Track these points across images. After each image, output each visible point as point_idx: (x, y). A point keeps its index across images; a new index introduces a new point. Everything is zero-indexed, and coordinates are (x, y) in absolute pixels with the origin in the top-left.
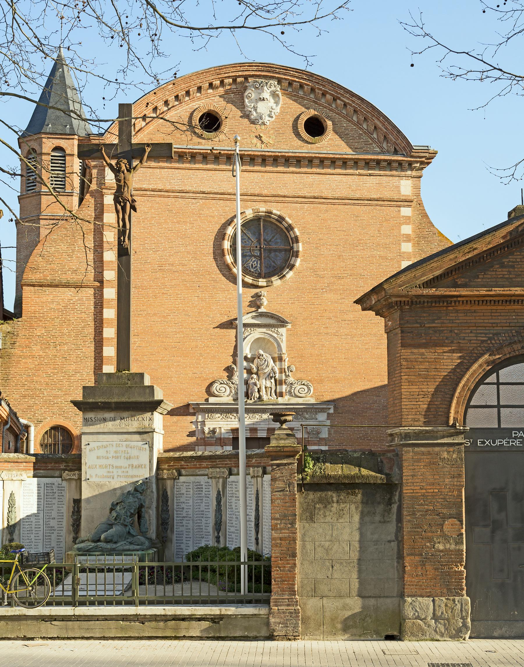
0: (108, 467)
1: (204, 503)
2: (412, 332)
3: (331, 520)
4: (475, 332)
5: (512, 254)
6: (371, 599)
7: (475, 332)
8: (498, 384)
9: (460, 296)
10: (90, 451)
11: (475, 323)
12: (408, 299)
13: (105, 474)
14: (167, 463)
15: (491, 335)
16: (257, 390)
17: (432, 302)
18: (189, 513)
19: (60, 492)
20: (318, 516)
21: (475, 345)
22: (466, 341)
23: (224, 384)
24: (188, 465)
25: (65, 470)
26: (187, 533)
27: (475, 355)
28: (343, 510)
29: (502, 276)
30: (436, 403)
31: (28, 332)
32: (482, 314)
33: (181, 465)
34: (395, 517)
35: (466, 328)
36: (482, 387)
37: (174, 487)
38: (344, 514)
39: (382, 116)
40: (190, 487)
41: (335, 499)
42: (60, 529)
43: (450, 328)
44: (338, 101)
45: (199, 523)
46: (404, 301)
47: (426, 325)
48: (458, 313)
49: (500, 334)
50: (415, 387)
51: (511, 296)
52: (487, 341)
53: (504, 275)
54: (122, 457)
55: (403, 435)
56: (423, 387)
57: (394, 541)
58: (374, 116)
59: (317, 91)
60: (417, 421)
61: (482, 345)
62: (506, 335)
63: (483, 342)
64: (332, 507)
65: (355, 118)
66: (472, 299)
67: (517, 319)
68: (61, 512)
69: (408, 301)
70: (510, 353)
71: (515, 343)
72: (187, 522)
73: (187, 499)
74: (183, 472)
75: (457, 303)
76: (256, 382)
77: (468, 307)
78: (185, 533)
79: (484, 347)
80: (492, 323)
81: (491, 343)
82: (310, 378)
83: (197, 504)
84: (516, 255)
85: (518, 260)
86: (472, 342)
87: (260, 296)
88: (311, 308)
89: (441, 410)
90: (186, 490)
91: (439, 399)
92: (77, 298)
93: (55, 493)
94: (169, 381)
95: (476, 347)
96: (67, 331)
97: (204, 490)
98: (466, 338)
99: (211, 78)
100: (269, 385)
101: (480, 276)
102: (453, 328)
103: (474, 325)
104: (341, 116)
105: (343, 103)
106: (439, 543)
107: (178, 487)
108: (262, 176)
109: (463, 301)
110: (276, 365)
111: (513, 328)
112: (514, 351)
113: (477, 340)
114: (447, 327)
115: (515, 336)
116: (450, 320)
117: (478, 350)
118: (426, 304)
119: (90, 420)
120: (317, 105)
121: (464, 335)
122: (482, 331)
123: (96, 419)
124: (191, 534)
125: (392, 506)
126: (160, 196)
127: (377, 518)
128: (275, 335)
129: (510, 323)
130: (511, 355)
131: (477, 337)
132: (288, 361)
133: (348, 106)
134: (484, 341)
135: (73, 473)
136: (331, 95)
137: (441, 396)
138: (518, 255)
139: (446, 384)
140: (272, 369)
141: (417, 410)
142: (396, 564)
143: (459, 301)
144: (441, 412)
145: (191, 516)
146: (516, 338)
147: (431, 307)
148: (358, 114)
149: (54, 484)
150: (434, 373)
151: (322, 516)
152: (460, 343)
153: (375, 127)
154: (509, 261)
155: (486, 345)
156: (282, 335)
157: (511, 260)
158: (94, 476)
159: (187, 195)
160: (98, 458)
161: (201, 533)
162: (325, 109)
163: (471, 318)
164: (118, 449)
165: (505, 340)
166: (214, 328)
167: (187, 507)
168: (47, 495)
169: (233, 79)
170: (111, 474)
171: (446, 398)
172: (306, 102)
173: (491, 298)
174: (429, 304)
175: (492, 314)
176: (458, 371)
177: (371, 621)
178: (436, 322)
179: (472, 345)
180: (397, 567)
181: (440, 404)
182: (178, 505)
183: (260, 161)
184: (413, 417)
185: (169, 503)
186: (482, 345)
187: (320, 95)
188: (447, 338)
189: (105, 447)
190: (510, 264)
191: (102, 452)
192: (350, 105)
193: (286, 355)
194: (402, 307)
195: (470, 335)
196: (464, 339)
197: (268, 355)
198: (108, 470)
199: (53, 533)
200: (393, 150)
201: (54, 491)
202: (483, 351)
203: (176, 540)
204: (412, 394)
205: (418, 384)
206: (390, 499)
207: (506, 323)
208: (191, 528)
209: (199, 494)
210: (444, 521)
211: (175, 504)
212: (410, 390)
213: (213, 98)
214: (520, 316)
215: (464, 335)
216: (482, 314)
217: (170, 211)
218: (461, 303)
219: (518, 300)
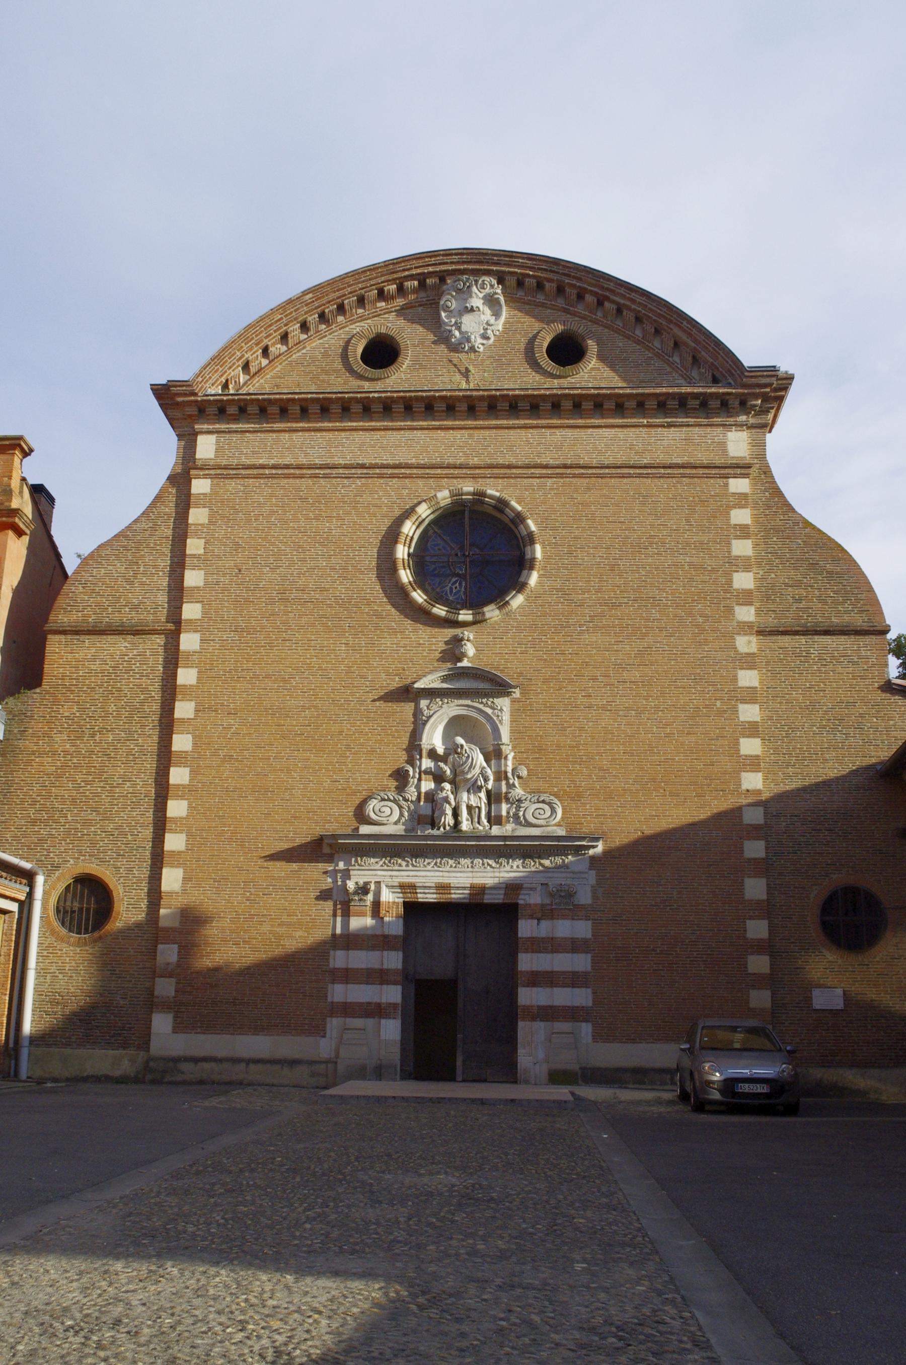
16: (449, 811)
23: (389, 800)
59: (568, 290)
65: (639, 332)
76: (447, 797)
82: (556, 790)
87: (462, 639)
88: (559, 661)
92: (135, 652)
100: (474, 802)
105: (615, 307)
108: (470, 436)
110: (489, 766)
128: (489, 711)
132: (514, 758)
140: (481, 773)
156: (501, 710)
166: (374, 701)
187: (574, 297)
192: (629, 309)
193: (510, 747)
197: (473, 746)
213: (386, 316)
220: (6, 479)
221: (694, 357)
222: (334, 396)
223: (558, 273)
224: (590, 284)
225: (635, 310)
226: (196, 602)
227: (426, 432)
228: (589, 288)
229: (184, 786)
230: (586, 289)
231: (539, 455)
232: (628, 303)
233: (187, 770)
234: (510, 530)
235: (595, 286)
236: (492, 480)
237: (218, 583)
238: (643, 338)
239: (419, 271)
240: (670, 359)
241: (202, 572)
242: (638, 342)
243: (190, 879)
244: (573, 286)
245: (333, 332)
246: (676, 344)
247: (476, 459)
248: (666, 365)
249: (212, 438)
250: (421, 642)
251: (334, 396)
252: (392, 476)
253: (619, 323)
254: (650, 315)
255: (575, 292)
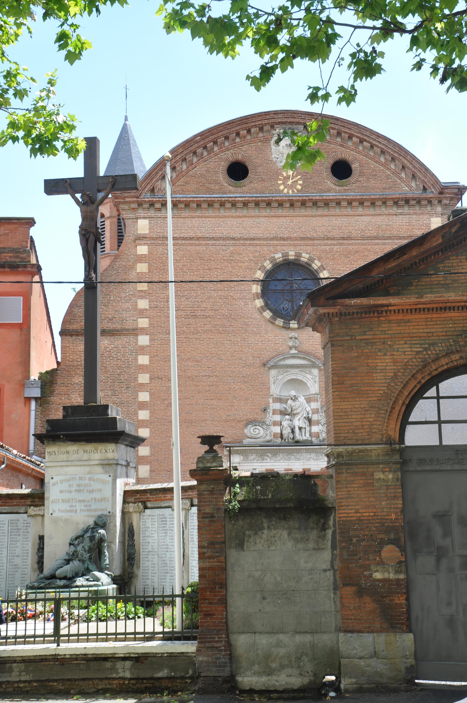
0: (71, 501)
1: (168, 536)
2: (343, 345)
3: (261, 548)
4: (409, 342)
5: (448, 258)
6: (307, 635)
7: (409, 342)
8: (438, 398)
9: (390, 305)
10: (53, 485)
11: (409, 333)
12: (336, 311)
13: (68, 509)
14: (134, 496)
15: (427, 346)
17: (361, 313)
18: (155, 547)
19: (25, 528)
20: (249, 544)
21: (410, 357)
22: (400, 353)
24: (153, 498)
25: (30, 506)
26: (153, 569)
27: (410, 367)
28: (275, 537)
29: (437, 282)
30: (370, 420)
31: (66, 380)
32: (416, 324)
33: (147, 498)
34: (329, 543)
35: (400, 339)
36: (421, 401)
37: (140, 521)
38: (276, 541)
39: (409, 155)
40: (155, 520)
41: (265, 525)
42: (25, 567)
43: (382, 340)
44: (365, 143)
45: (164, 557)
46: (333, 313)
47: (357, 338)
48: (390, 323)
49: (436, 344)
50: (347, 403)
51: (446, 303)
52: (422, 351)
53: (439, 281)
54: (85, 491)
55: (335, 455)
56: (355, 403)
57: (329, 570)
58: (401, 155)
59: (343, 134)
60: (350, 439)
61: (417, 357)
62: (444, 345)
63: (418, 353)
64: (263, 533)
65: (382, 159)
66: (403, 308)
67: (454, 327)
68: (26, 549)
69: (337, 313)
70: (447, 364)
71: (452, 353)
72: (152, 556)
73: (153, 532)
74: (149, 505)
75: (389, 313)
77: (400, 317)
78: (150, 568)
79: (420, 358)
80: (427, 333)
81: (427, 354)
83: (162, 538)
84: (452, 259)
85: (454, 264)
86: (406, 353)
89: (375, 426)
90: (151, 523)
91: (373, 416)
92: (113, 346)
93: (20, 529)
94: (203, 424)
95: (411, 359)
96: (104, 378)
97: (168, 523)
98: (400, 350)
99: (238, 128)
101: (414, 284)
102: (386, 340)
103: (408, 335)
104: (368, 158)
105: (370, 145)
106: (377, 571)
107: (144, 520)
108: (292, 221)
109: (395, 310)
111: (450, 337)
112: (452, 361)
113: (411, 351)
114: (380, 339)
115: (452, 345)
116: (382, 331)
117: (413, 362)
118: (355, 315)
119: (53, 453)
120: (343, 149)
121: (398, 346)
122: (416, 342)
123: (60, 452)
124: (156, 569)
125: (327, 532)
126: (191, 245)
127: (311, 545)
129: (446, 332)
130: (449, 366)
131: (411, 348)
133: (375, 148)
134: (419, 352)
135: (38, 508)
136: (357, 137)
137: (374, 412)
138: (454, 259)
139: (380, 400)
141: (349, 428)
142: (332, 595)
143: (390, 311)
144: (375, 429)
145: (156, 550)
146: (454, 348)
147: (361, 318)
148: (385, 155)
149: (18, 520)
150: (367, 388)
151: (253, 543)
152: (394, 355)
153: (403, 167)
154: (445, 266)
155: (421, 356)
157: (447, 265)
158: (57, 511)
159: (218, 242)
160: (61, 492)
161: (166, 568)
162: (352, 152)
163: (404, 328)
164: (81, 482)
165: (442, 350)
167: (152, 541)
168: (11, 532)
169: (259, 128)
170: (74, 508)
171: (380, 414)
172: (332, 145)
173: (425, 306)
174: (359, 315)
175: (427, 323)
176: (392, 384)
177: (308, 660)
178: (368, 333)
179: (406, 357)
180: (334, 599)
181: (374, 420)
182: (144, 540)
183: (288, 205)
184: (345, 435)
185: (135, 538)
186: (417, 357)
187: (346, 138)
188: (380, 351)
189: (68, 481)
190: (446, 269)
191: (65, 486)
192: (377, 146)
194: (330, 319)
195: (404, 346)
196: (398, 351)
198: (71, 504)
199: (17, 571)
200: (422, 187)
201: (19, 528)
202: (419, 362)
203: (142, 576)
204: (344, 410)
205: (350, 400)
206: (324, 524)
207: (442, 332)
208: (157, 563)
209: (163, 527)
210: (382, 548)
211: (141, 538)
212: (341, 407)
213: (241, 148)
214: (457, 324)
215: (398, 346)
216: (416, 324)
217: (201, 258)
218: (393, 312)
219: (454, 307)
220: (24, 243)
221: (413, 175)
222: (216, 199)
223: (338, 125)
224: (356, 132)
225: (380, 147)
226: (145, 318)
227: (267, 218)
228: (355, 134)
229: (147, 421)
230: (354, 135)
231: (329, 232)
232: (377, 144)
233: (148, 412)
234: (307, 268)
235: (359, 133)
236: (305, 247)
237: (157, 307)
238: (385, 163)
239: (260, 123)
240: (400, 176)
241: (147, 300)
242: (383, 165)
243: (154, 471)
244: (345, 132)
245: (212, 158)
246: (403, 167)
247: (295, 235)
248: (397, 179)
249: (146, 222)
250: (270, 339)
251: (216, 199)
252: (250, 245)
253: (371, 153)
254: (389, 151)
255: (347, 136)
